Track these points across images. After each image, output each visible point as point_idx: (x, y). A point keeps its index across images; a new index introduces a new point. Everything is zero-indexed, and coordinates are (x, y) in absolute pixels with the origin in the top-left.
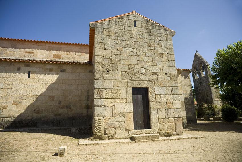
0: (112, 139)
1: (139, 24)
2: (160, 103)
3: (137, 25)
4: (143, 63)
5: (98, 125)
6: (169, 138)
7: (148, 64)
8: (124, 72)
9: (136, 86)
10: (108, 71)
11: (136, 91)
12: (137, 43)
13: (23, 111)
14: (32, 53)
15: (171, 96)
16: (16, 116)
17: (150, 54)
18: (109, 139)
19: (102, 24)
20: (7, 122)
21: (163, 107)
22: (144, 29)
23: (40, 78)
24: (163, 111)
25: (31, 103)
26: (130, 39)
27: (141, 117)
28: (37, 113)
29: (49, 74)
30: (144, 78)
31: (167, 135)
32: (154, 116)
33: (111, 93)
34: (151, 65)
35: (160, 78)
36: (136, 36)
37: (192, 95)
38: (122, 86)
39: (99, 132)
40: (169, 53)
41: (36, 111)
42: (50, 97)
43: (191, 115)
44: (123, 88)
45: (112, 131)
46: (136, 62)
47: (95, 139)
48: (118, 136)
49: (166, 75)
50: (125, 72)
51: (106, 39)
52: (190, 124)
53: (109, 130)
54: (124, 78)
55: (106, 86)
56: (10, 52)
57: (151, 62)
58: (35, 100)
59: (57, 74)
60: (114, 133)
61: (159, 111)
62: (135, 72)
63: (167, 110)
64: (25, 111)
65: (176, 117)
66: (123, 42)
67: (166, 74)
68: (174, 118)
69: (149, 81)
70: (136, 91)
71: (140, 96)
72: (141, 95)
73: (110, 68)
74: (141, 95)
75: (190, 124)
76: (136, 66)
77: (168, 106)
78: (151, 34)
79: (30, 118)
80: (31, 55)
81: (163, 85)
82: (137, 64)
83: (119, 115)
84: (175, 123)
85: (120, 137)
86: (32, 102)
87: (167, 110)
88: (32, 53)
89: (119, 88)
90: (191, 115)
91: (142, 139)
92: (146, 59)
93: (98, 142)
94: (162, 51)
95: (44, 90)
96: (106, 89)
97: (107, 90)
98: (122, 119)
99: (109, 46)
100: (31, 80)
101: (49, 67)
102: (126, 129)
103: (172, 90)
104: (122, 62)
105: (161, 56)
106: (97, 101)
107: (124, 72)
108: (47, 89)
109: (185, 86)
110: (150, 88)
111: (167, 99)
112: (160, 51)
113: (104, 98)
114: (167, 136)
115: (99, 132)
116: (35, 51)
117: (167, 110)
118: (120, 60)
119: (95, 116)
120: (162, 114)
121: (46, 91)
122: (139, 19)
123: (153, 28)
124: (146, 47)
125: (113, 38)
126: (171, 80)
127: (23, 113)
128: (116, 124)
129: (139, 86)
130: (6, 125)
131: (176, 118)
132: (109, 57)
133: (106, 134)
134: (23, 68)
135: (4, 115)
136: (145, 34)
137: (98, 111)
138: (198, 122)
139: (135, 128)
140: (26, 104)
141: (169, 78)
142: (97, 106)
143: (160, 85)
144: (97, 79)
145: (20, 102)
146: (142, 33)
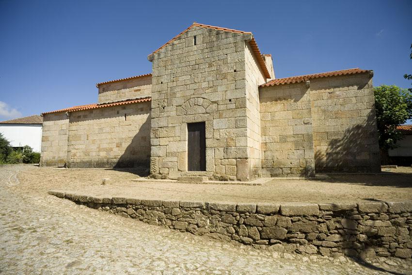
0: (165, 178)
1: (199, 40)
2: (218, 140)
3: (197, 43)
4: (201, 91)
5: (153, 165)
6: (223, 182)
7: (207, 91)
8: (179, 106)
9: (191, 122)
10: (164, 108)
11: (192, 127)
12: (195, 67)
13: (123, 152)
14: (140, 90)
15: (235, 130)
16: (119, 157)
17: (210, 78)
18: (162, 179)
19: (159, 54)
20: (114, 163)
21: (222, 145)
22: (205, 45)
23: (134, 119)
24: (222, 149)
25: (128, 145)
26: (188, 64)
27: (197, 158)
28: (134, 154)
29: (140, 114)
30: (201, 110)
31: (223, 179)
32: (209, 154)
33: (165, 132)
34: (210, 91)
35: (222, 107)
36: (194, 58)
37: (373, 119)
38: (176, 123)
39: (154, 172)
40: (237, 70)
41: (133, 153)
42: (142, 137)
43: (368, 157)
44: (177, 125)
45: (165, 171)
46: (193, 92)
47: (151, 177)
48: (170, 176)
49: (230, 103)
50: (180, 106)
51: (163, 70)
52: (371, 173)
53: (162, 170)
54: (179, 113)
55: (162, 124)
56: (123, 93)
57: (210, 89)
58: (131, 141)
59: (147, 113)
60: (167, 173)
61: (217, 150)
62: (191, 104)
63: (226, 149)
64: (125, 153)
65: (239, 158)
66: (179, 70)
67: (230, 100)
68: (236, 158)
69: (207, 113)
70: (192, 127)
71: (197, 133)
72: (197, 130)
73: (166, 104)
74: (197, 130)
75: (371, 173)
76: (192, 97)
77: (228, 143)
78: (214, 49)
79: (128, 159)
80: (139, 92)
81: (224, 116)
82: (194, 94)
83: (173, 154)
84: (236, 165)
85: (172, 177)
86: (129, 143)
87: (226, 149)
88: (140, 90)
89: (173, 125)
90: (368, 157)
91: (185, 181)
92: (205, 85)
93: (153, 180)
94: (227, 69)
95: (138, 131)
96: (161, 128)
97: (162, 129)
98: (175, 159)
99: (164, 79)
100: (127, 122)
101: (140, 106)
102: (179, 170)
103: (236, 121)
104: (178, 95)
105: (225, 77)
106: (154, 141)
107: (179, 106)
108: (140, 130)
109: (358, 104)
110: (206, 122)
111: (228, 134)
112: (225, 70)
113: (159, 138)
114: (222, 180)
115: (154, 172)
116: (142, 87)
117: (227, 149)
118: (174, 93)
119: (152, 155)
120: (220, 153)
121: (139, 132)
122: (200, 32)
123: (218, 39)
124: (207, 70)
125: (170, 67)
126: (236, 108)
127: (124, 155)
128: (170, 164)
129: (194, 121)
130: (114, 165)
131: (238, 159)
132: (164, 92)
133: (160, 173)
134: (122, 111)
135: (111, 157)
136: (206, 51)
137: (154, 150)
138: (383, 170)
139: (190, 169)
140: (125, 145)
141: (233, 106)
142: (154, 146)
143: (220, 117)
144: (154, 118)
145: (121, 145)
146: (202, 50)
